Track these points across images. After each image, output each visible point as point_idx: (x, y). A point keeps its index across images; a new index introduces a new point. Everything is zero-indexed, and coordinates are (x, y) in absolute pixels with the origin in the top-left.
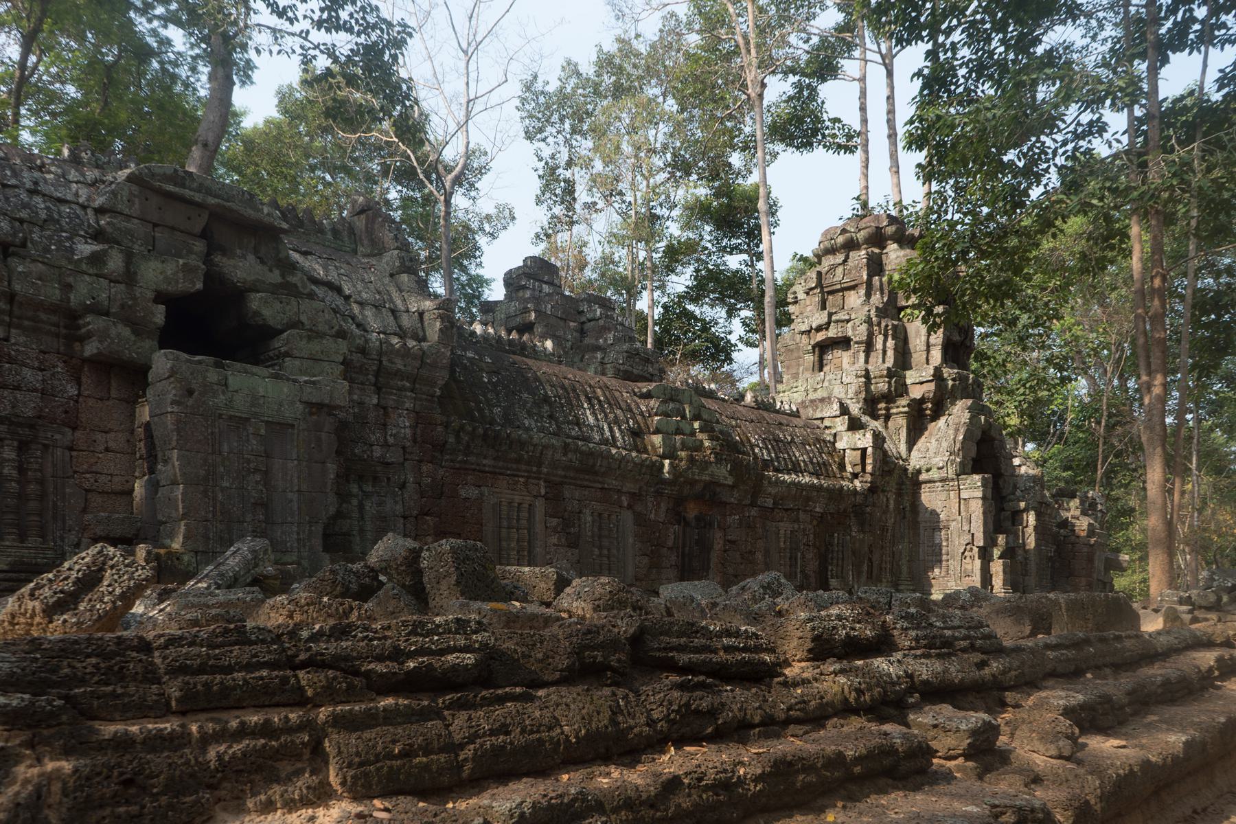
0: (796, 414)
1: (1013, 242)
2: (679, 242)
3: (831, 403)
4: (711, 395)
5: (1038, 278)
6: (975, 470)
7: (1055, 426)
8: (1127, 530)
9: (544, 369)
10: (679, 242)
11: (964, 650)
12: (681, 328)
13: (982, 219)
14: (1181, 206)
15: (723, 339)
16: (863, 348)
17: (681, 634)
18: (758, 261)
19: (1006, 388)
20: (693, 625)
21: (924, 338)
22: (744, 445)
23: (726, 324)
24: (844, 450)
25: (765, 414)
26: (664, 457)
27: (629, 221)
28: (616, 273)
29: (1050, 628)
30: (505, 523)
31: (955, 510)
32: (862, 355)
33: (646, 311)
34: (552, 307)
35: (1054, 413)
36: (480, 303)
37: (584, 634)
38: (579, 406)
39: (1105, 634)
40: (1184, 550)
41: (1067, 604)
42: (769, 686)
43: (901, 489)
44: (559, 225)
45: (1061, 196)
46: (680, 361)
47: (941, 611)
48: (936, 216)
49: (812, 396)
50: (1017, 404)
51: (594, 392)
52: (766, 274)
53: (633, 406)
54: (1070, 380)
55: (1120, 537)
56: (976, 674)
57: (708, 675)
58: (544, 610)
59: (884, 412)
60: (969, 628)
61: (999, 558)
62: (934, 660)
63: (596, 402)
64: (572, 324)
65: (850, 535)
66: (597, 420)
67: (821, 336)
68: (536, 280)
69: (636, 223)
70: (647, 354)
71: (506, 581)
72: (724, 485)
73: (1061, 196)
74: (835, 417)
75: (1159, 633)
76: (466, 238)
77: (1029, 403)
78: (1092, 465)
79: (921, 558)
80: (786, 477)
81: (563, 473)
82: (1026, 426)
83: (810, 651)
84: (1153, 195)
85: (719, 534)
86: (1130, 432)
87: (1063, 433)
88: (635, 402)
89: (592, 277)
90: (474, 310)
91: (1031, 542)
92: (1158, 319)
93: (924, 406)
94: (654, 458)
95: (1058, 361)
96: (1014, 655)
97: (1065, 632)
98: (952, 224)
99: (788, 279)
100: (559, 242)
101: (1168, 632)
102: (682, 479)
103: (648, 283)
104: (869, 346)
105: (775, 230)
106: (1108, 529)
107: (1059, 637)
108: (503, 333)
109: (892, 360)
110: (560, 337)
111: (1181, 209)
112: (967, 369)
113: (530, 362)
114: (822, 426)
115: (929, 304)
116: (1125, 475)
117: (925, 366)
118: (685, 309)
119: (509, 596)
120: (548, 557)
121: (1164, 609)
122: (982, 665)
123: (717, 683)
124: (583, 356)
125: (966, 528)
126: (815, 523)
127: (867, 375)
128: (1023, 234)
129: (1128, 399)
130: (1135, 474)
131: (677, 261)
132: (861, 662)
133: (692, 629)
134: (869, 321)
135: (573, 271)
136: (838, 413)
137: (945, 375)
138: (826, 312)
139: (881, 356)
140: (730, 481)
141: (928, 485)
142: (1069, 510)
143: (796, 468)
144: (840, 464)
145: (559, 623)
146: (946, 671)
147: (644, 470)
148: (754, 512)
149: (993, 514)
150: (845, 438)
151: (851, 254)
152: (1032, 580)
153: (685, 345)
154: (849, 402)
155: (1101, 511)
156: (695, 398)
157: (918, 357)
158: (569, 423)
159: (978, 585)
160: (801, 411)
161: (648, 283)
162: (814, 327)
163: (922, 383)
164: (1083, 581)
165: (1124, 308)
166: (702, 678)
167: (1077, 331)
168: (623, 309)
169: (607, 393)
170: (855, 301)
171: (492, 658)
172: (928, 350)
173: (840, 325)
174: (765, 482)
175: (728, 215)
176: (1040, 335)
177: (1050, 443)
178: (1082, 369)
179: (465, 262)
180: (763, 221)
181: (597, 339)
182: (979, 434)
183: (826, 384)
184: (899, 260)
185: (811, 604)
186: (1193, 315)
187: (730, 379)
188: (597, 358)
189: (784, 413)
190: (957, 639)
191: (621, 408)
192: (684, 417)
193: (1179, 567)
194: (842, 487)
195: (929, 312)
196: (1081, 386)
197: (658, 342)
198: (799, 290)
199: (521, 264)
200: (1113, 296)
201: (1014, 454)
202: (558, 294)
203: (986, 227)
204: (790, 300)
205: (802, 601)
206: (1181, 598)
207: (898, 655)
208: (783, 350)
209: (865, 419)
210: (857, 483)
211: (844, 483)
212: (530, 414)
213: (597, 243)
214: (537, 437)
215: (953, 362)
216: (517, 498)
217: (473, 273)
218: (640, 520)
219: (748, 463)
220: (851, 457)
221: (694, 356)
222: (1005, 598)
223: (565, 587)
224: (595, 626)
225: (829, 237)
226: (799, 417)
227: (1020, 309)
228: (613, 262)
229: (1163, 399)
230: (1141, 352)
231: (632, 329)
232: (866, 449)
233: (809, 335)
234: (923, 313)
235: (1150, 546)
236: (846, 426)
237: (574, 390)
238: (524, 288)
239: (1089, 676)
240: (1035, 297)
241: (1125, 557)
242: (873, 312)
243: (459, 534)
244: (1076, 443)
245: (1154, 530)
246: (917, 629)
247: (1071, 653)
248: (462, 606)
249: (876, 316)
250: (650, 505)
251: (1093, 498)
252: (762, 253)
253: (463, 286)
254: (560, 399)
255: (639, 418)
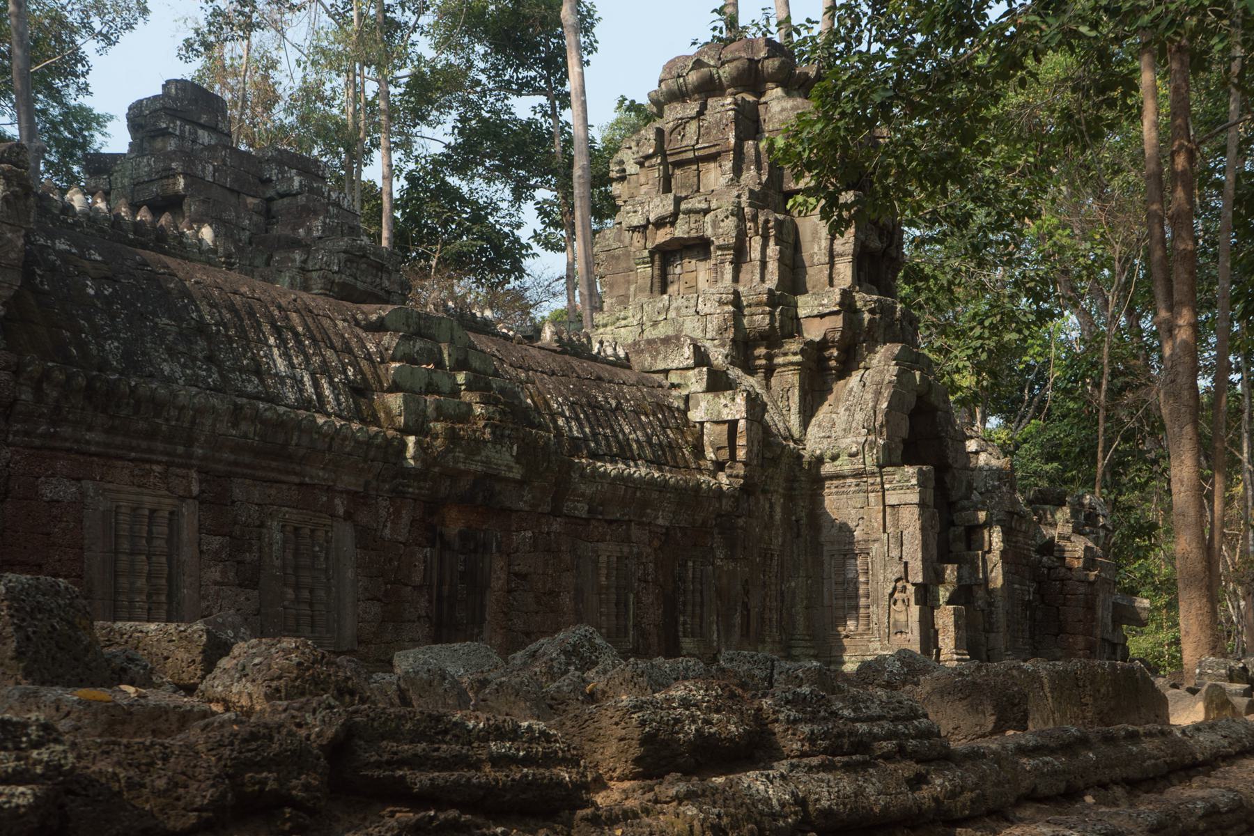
0: (625, 364)
1: (959, 91)
2: (433, 69)
3: (680, 346)
4: (485, 328)
5: (1001, 150)
6: (907, 460)
7: (1031, 389)
8: (1146, 558)
9: (197, 276)
10: (433, 69)
11: (888, 757)
12: (438, 215)
13: (913, 52)
14: (1215, 40)
15: (507, 235)
16: (730, 257)
17: (416, 737)
18: (563, 108)
19: (951, 325)
20: (438, 719)
21: (824, 244)
22: (540, 413)
23: (512, 210)
24: (702, 423)
25: (575, 362)
26: (406, 431)
27: (349, 28)
28: (326, 116)
29: (1025, 718)
30: (125, 546)
31: (877, 524)
32: (728, 269)
33: (379, 184)
34: (215, 170)
35: (1029, 368)
36: (86, 155)
37: (245, 741)
38: (259, 341)
39: (1111, 729)
40: (1235, 591)
41: (1052, 680)
42: (569, 825)
43: (792, 489)
44: (226, 29)
45: (1033, 18)
46: (438, 271)
47: (854, 690)
48: (843, 45)
49: (650, 334)
50: (970, 352)
51: (287, 318)
52: (577, 131)
53: (354, 343)
54: (1051, 315)
55: (1134, 570)
56: (909, 798)
57: (464, 807)
58: (186, 701)
59: (763, 362)
60: (896, 719)
61: (948, 603)
62: (839, 774)
63: (290, 335)
64: (250, 200)
65: (713, 564)
66: (292, 365)
67: (663, 236)
68: (186, 121)
69: (360, 33)
70: (381, 257)
71: (112, 649)
72: (507, 480)
73: (1033, 18)
74: (687, 369)
75: (1197, 728)
76: (58, 38)
77: (990, 352)
78: (1088, 453)
79: (826, 602)
80: (609, 467)
81: (232, 457)
82: (986, 389)
83: (637, 761)
84: (1173, 21)
85: (499, 563)
86: (1145, 401)
87: (1044, 401)
88: (357, 336)
89: (287, 121)
90: (76, 168)
91: (997, 577)
92: (1182, 220)
93: (827, 354)
94: (390, 433)
95: (1032, 284)
96: (968, 765)
97: (1051, 725)
98: (868, 60)
99: (611, 140)
100: (227, 57)
101: (1212, 727)
102: (437, 469)
103: (382, 137)
104: (739, 254)
105: (590, 57)
106: (1116, 556)
107: (1040, 733)
108: (124, 211)
109: (776, 278)
110: (229, 222)
111: (1217, 44)
112: (893, 295)
113: (172, 263)
114: (666, 383)
115: (831, 188)
116: (1140, 470)
117: (828, 288)
118: (444, 183)
119: (120, 675)
120: (204, 604)
121: (1204, 689)
122: (918, 781)
123: (479, 821)
124: (271, 257)
125: (895, 553)
126: (656, 543)
127: (736, 301)
128: (976, 80)
129: (1140, 348)
130: (1155, 468)
131: (430, 102)
132: (720, 780)
133: (437, 728)
134: (738, 213)
135: (253, 109)
136: (691, 362)
137: (859, 304)
138: (671, 196)
139: (758, 271)
140: (517, 473)
141: (835, 482)
142: (1054, 525)
143: (624, 453)
144: (695, 447)
145: (202, 723)
146: (860, 792)
147: (372, 454)
148: (556, 526)
149: (937, 529)
150: (703, 404)
151: (710, 102)
152: (1000, 640)
153: (445, 243)
154: (708, 344)
155: (1104, 526)
156: (459, 332)
157: (816, 274)
158: (242, 370)
159: (916, 647)
160: (633, 358)
161: (382, 137)
162: (652, 219)
163: (822, 316)
164: (1081, 641)
165: (1133, 203)
166: (453, 813)
167: (1062, 237)
168: (339, 178)
169: (309, 321)
170: (716, 179)
171: (69, 792)
172: (832, 263)
173: (693, 217)
174: (575, 476)
175: (514, 28)
176: (1004, 242)
177: (1023, 417)
178: (1070, 299)
179: (58, 83)
180: (569, 40)
181: (294, 229)
182: (911, 400)
183: (672, 314)
184: (785, 114)
185: (643, 681)
186: (1236, 215)
187: (520, 304)
188: (294, 261)
189: (605, 361)
190: (876, 738)
191: (333, 347)
192: (439, 364)
193: (1229, 619)
194: (699, 484)
195: (832, 201)
196: (1070, 326)
197: (400, 236)
198: (629, 158)
199: (159, 91)
200: (1117, 182)
201: (968, 433)
202: (225, 147)
203: (919, 66)
204: (613, 175)
205: (628, 675)
206: (1231, 670)
207: (782, 767)
208: (602, 256)
209: (734, 372)
210: (723, 478)
211: (702, 479)
212: (172, 353)
213: (293, 64)
214: (185, 394)
215: (871, 282)
216: (149, 501)
217: (73, 103)
218: (366, 539)
219: (547, 444)
220: (713, 435)
221: (459, 263)
222: (954, 669)
223: (221, 656)
224: (266, 726)
225: (674, 73)
226: (629, 368)
227: (974, 200)
228: (321, 98)
229: (1192, 351)
230: (1158, 274)
231: (354, 214)
232: (736, 421)
233: (644, 232)
234: (823, 202)
235: (1180, 585)
236: (704, 384)
237: (252, 314)
238: (165, 133)
239: (1089, 799)
240: (996, 182)
241: (1143, 603)
242: (744, 198)
243: (40, 566)
244: (1064, 416)
245: (1185, 558)
246: (812, 721)
247: (1058, 762)
248: (24, 696)
249: (750, 205)
250: (383, 513)
251: (1091, 507)
252: (568, 94)
253: (54, 126)
254: (227, 329)
255: (364, 364)
